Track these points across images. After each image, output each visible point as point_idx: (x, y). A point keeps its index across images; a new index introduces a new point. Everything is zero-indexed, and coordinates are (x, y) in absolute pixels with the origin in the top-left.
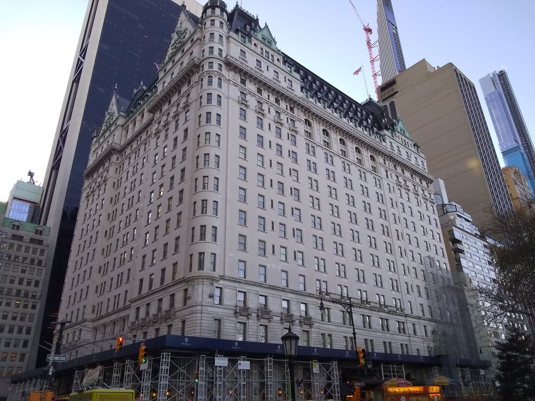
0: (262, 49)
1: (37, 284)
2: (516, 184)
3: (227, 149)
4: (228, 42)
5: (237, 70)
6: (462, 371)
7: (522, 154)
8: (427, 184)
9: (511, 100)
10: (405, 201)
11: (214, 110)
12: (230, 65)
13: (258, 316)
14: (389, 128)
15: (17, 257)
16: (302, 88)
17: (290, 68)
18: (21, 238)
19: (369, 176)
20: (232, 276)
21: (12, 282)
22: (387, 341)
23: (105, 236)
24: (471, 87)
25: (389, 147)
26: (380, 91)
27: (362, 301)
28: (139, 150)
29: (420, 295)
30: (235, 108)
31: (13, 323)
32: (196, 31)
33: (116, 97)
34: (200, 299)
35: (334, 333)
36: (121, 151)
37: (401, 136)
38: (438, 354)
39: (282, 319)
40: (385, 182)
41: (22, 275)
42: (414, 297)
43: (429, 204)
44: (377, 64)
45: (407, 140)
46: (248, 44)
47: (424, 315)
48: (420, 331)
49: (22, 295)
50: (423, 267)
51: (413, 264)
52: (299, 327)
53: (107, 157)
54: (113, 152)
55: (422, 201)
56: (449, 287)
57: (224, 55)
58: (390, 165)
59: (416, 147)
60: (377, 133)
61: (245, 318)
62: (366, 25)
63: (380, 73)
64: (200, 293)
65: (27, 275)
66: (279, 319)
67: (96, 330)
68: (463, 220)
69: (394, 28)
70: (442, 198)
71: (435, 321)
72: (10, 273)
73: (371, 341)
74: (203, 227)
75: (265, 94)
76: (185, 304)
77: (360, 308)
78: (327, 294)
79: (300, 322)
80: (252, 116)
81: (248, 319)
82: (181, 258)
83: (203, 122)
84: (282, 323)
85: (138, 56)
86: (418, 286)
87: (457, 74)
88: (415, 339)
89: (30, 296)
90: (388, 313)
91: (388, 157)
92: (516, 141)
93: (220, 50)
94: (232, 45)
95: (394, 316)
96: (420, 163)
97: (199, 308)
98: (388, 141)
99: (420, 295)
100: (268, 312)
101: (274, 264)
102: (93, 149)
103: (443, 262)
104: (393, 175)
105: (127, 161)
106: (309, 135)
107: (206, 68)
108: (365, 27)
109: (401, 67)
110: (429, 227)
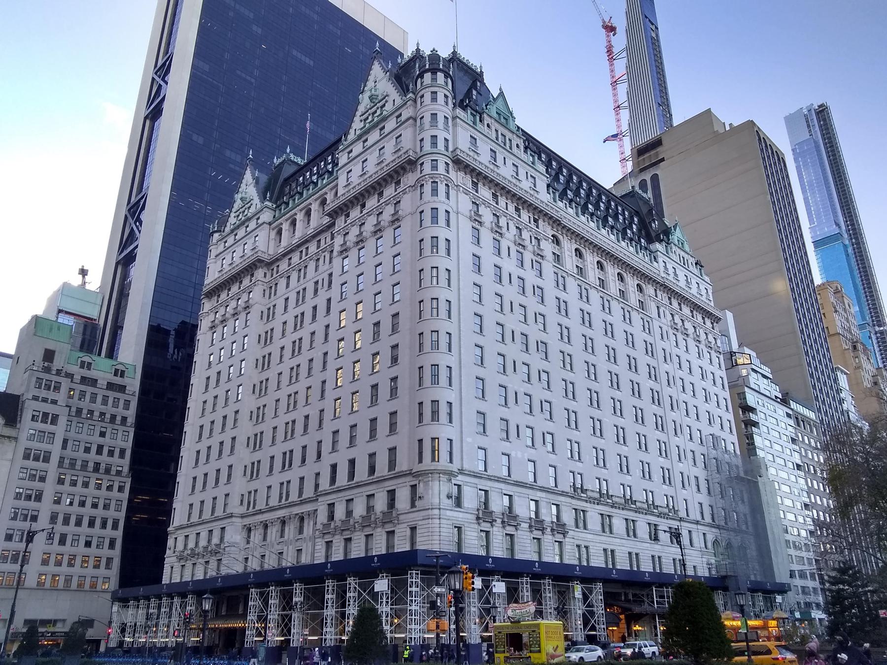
0: (497, 131)
1: (122, 452)
2: (836, 311)
3: (459, 289)
4: (455, 125)
5: (462, 166)
6: (753, 597)
7: (845, 246)
8: (712, 323)
9: (834, 155)
10: (681, 351)
11: (442, 233)
12: (459, 163)
13: (503, 522)
14: (662, 241)
15: (91, 412)
16: (548, 186)
17: (533, 156)
18: (93, 382)
19: (636, 317)
20: (472, 470)
21: (87, 450)
22: (657, 554)
23: (254, 392)
24: (779, 159)
25: (662, 269)
26: (636, 154)
27: (626, 501)
28: (306, 267)
29: (699, 490)
30: (465, 226)
31: (94, 512)
32: (405, 104)
33: (253, 175)
34: (436, 501)
35: (591, 544)
36: (270, 264)
37: (678, 251)
38: (723, 574)
39: (530, 527)
40: (656, 324)
41: (101, 440)
42: (689, 493)
43: (680, 337)
44: (622, 89)
45: (686, 256)
46: (479, 126)
47: (703, 518)
48: (698, 541)
49: (78, 467)
50: (704, 450)
51: (690, 446)
52: (550, 537)
53: (247, 270)
54: (258, 264)
55: (705, 350)
56: (738, 478)
57: (451, 149)
58: (663, 297)
59: (699, 267)
60: (646, 249)
61: (489, 525)
62: (607, 20)
63: (626, 104)
64: (436, 491)
65: (107, 441)
66: (527, 525)
67: (249, 530)
68: (760, 376)
69: (654, 28)
70: (729, 340)
71: (718, 527)
72: (83, 437)
73: (637, 554)
74: (435, 402)
75: (502, 201)
76: (413, 505)
77: (623, 509)
78: (583, 491)
79: (552, 530)
80: (487, 236)
81: (492, 526)
82: (403, 442)
83: (427, 251)
84: (531, 531)
85: (253, 81)
86: (697, 478)
87: (760, 139)
88: (692, 552)
89: (113, 472)
90: (658, 517)
91: (662, 285)
92: (837, 225)
93: (446, 140)
94: (459, 129)
95: (665, 521)
96: (704, 292)
97: (436, 512)
98: (660, 260)
99: (699, 490)
100: (515, 517)
101: (520, 451)
102: (213, 253)
103: (731, 440)
104: (667, 312)
105: (283, 282)
106: (557, 258)
107: (427, 168)
108: (604, 22)
109: (661, 97)
110: (712, 390)
